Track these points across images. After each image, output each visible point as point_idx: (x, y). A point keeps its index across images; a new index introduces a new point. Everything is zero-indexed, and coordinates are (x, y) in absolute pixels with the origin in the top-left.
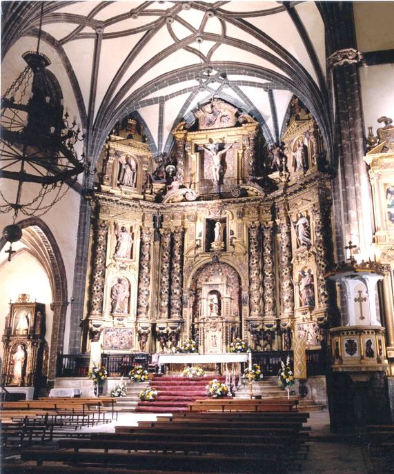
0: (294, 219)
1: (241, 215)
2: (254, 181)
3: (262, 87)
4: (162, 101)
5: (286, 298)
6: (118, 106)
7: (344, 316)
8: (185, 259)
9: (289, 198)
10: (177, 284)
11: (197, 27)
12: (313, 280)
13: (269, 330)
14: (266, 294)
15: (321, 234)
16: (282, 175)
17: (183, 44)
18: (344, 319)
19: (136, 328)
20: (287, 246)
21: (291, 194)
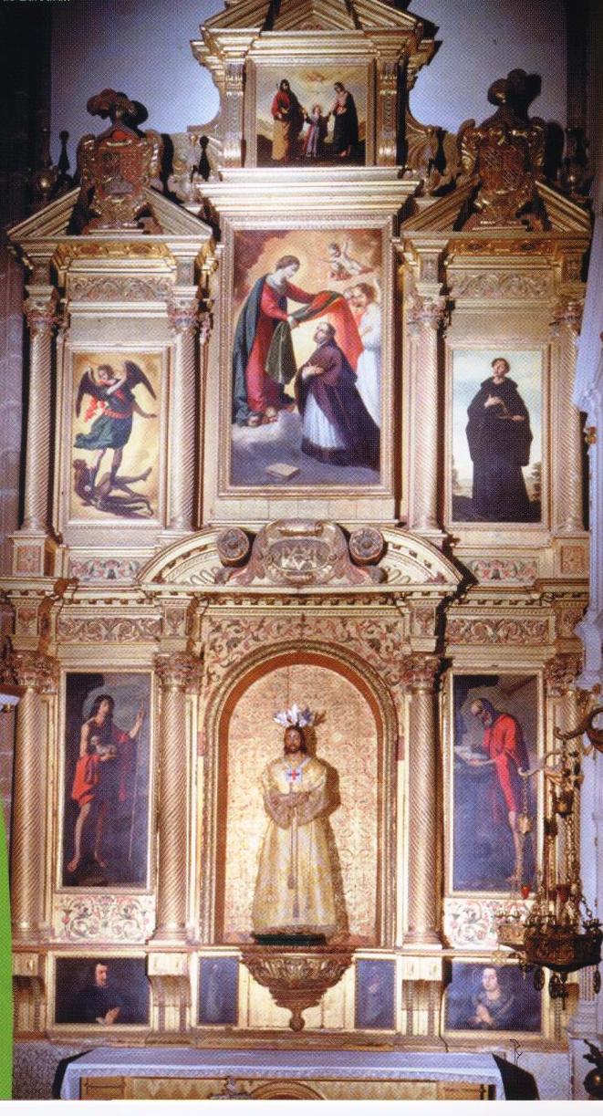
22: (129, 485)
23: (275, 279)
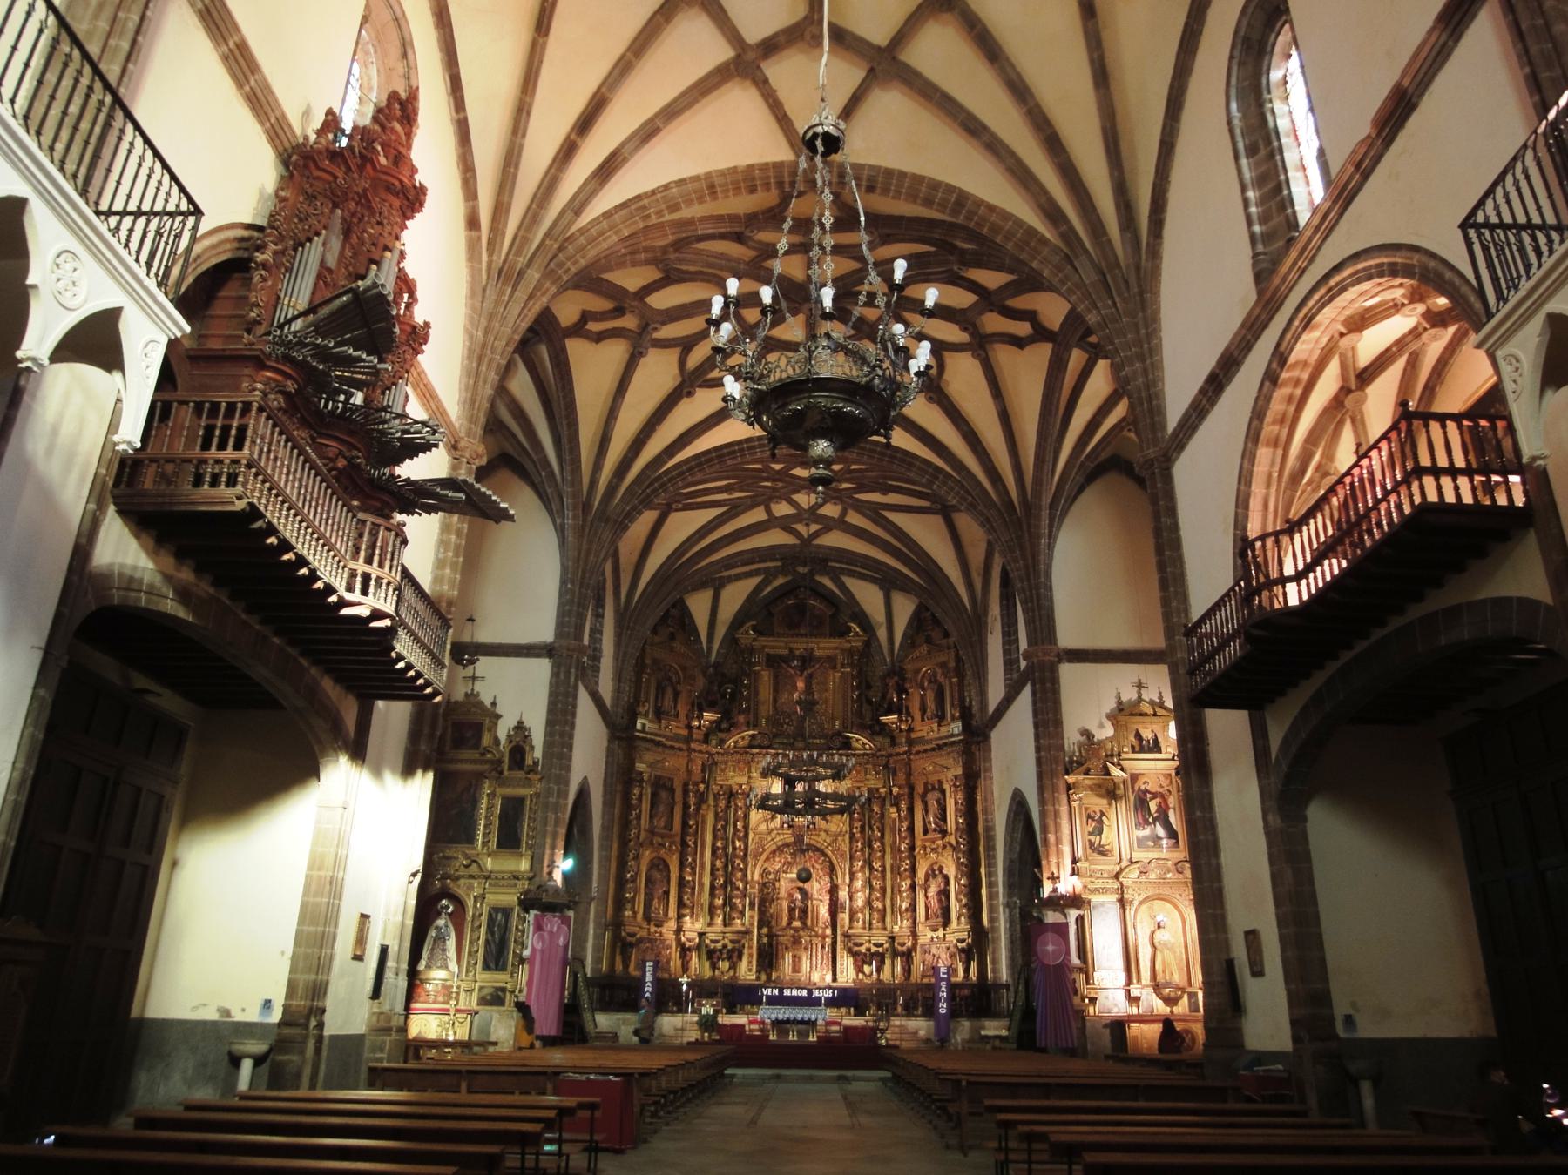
0: (920, 789)
4: (718, 586)
5: (905, 905)
8: (751, 835)
12: (947, 883)
14: (873, 897)
16: (900, 720)
17: (785, 524)
18: (993, 942)
19: (678, 941)
21: (918, 753)
22: (1025, 698)
23: (1143, 787)
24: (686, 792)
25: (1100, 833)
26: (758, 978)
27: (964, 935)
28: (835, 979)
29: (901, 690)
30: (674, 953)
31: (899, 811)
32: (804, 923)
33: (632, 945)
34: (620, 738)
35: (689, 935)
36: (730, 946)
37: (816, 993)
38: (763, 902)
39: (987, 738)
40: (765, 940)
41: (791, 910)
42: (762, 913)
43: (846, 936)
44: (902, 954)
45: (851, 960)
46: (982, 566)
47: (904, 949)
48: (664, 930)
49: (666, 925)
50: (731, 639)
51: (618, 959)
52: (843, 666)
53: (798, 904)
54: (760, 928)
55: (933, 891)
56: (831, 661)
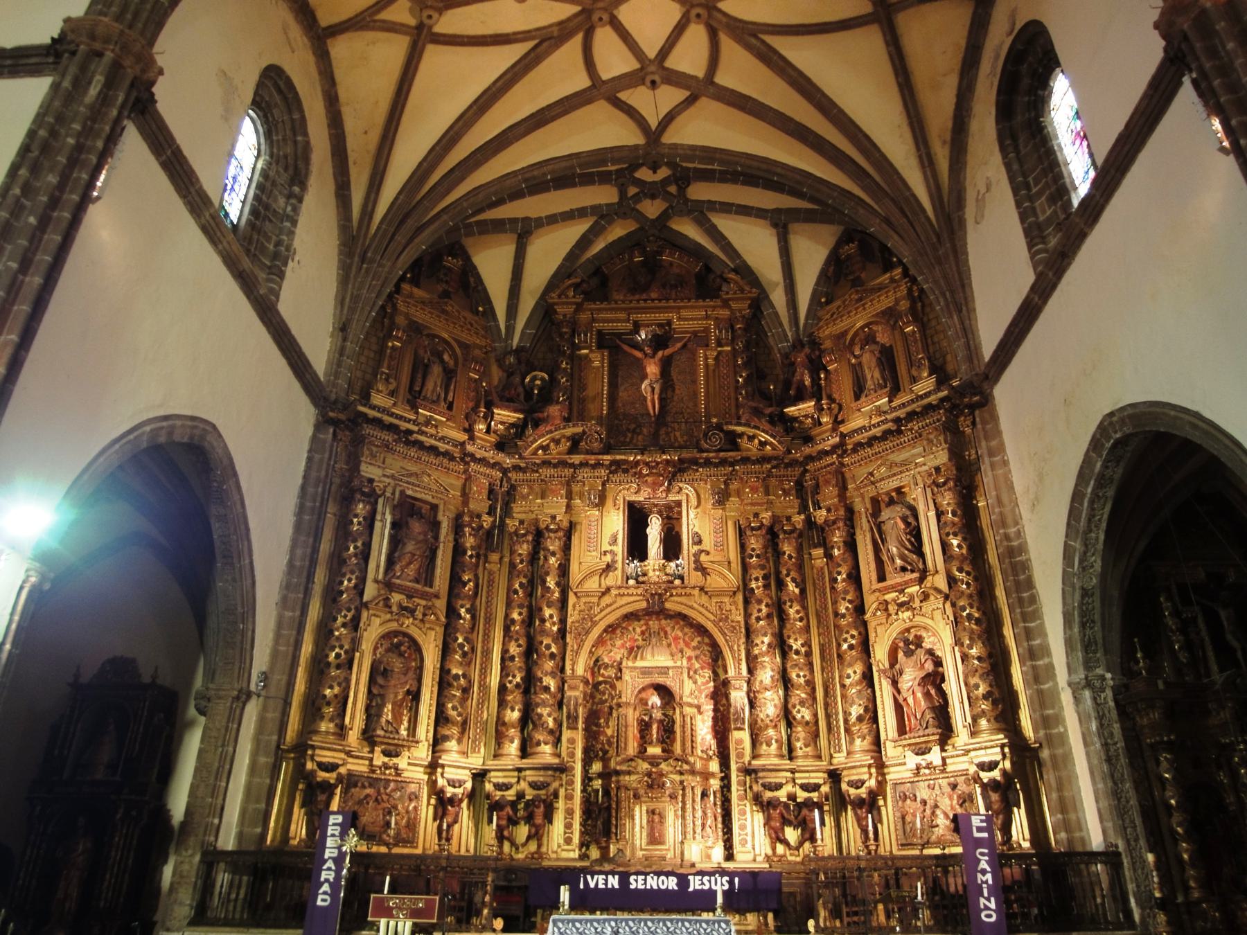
1: (722, 498)
2: (757, 412)
3: (764, 218)
4: (524, 231)
5: (856, 711)
6: (429, 217)
7: (1053, 757)
8: (572, 600)
9: (846, 460)
10: (551, 663)
11: (651, 53)
13: (808, 800)
15: (964, 539)
16: (819, 409)
19: (432, 784)
20: (849, 576)
24: (458, 528)
25: (812, 839)
26: (583, 857)
27: (994, 754)
28: (729, 857)
29: (816, 366)
30: (426, 812)
31: (828, 555)
32: (668, 752)
33: (328, 788)
34: (335, 423)
35: (451, 773)
36: (530, 794)
37: (695, 884)
38: (593, 719)
39: (986, 401)
40: (597, 784)
41: (644, 727)
42: (592, 734)
43: (748, 771)
44: (859, 803)
45: (759, 818)
46: (950, 124)
47: (863, 792)
48: (402, 762)
49: (406, 754)
50: (545, 310)
51: (298, 814)
52: (719, 344)
53: (658, 715)
54: (587, 763)
55: (910, 678)
56: (700, 339)
